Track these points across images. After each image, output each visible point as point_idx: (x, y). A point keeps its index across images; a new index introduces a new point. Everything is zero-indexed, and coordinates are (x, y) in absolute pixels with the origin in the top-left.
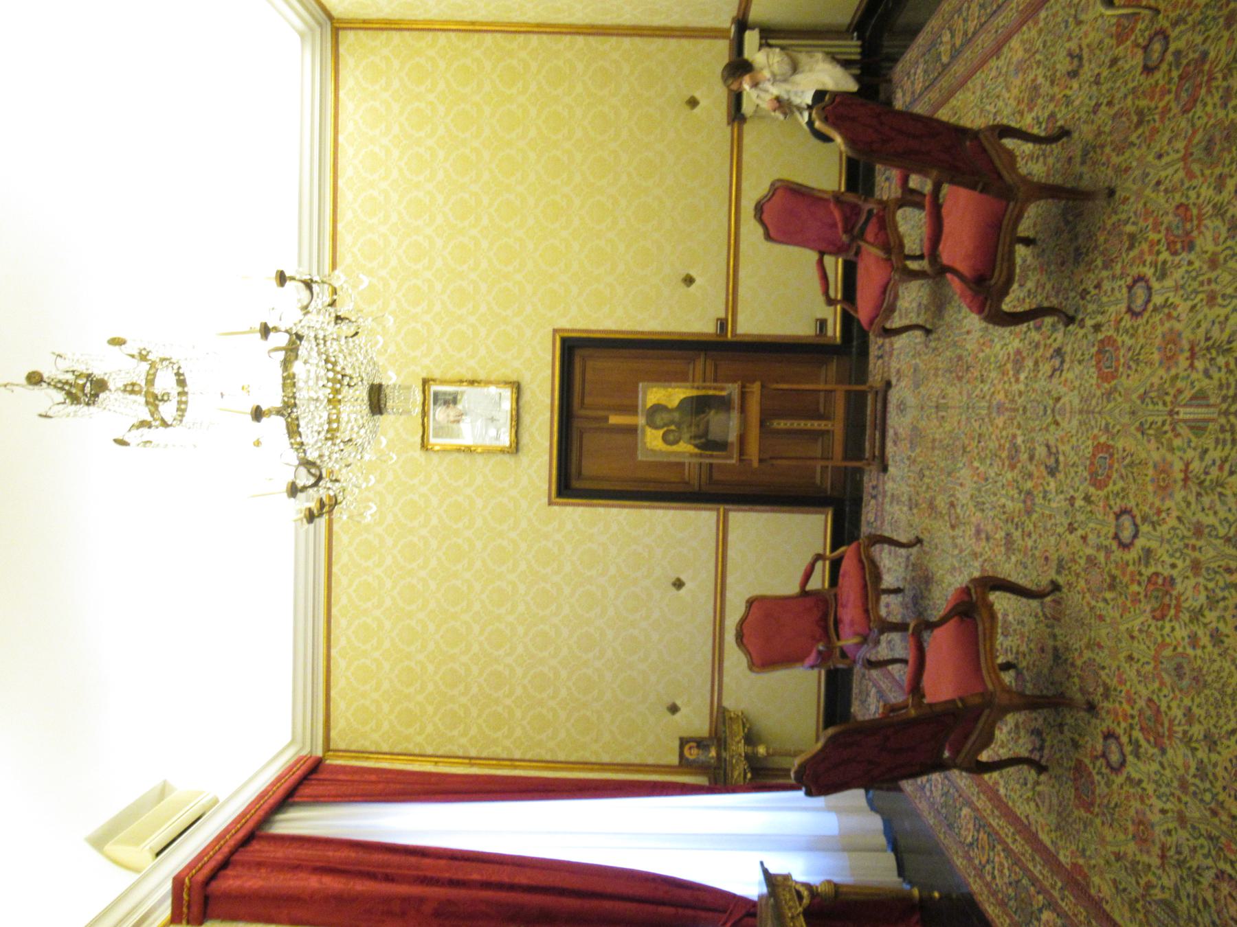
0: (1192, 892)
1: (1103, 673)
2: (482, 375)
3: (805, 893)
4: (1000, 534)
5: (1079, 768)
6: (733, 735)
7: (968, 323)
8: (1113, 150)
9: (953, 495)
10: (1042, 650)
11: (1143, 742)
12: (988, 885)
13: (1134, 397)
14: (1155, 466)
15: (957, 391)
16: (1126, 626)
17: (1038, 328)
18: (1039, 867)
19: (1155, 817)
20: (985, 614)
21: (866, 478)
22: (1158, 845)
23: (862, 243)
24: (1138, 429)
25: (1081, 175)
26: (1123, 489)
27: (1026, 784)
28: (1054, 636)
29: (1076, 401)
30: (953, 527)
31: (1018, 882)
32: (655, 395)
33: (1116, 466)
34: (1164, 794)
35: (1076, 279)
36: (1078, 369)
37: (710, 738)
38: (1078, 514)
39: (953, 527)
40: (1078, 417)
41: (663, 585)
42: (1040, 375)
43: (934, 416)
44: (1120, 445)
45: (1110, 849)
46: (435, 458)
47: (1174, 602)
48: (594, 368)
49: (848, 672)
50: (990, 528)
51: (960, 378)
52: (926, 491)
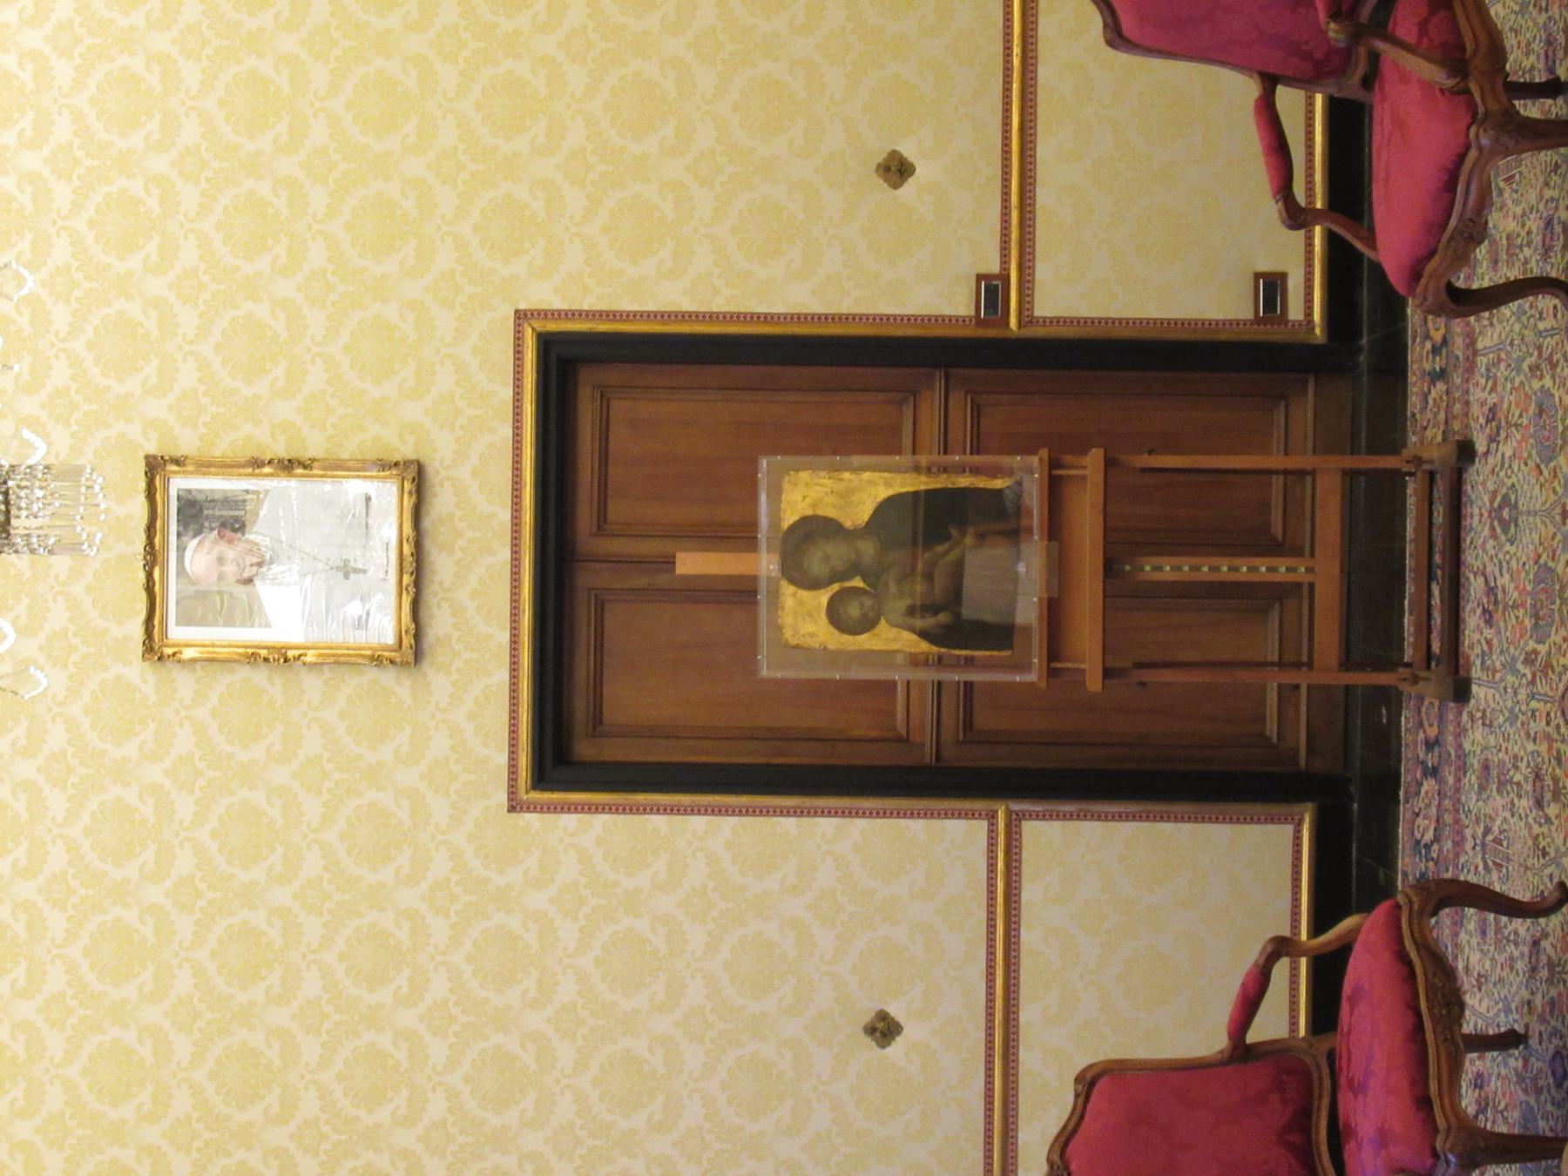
2: (314, 446)
21: (1406, 719)
23: (1380, 45)
32: (804, 492)
46: (184, 683)
48: (635, 424)
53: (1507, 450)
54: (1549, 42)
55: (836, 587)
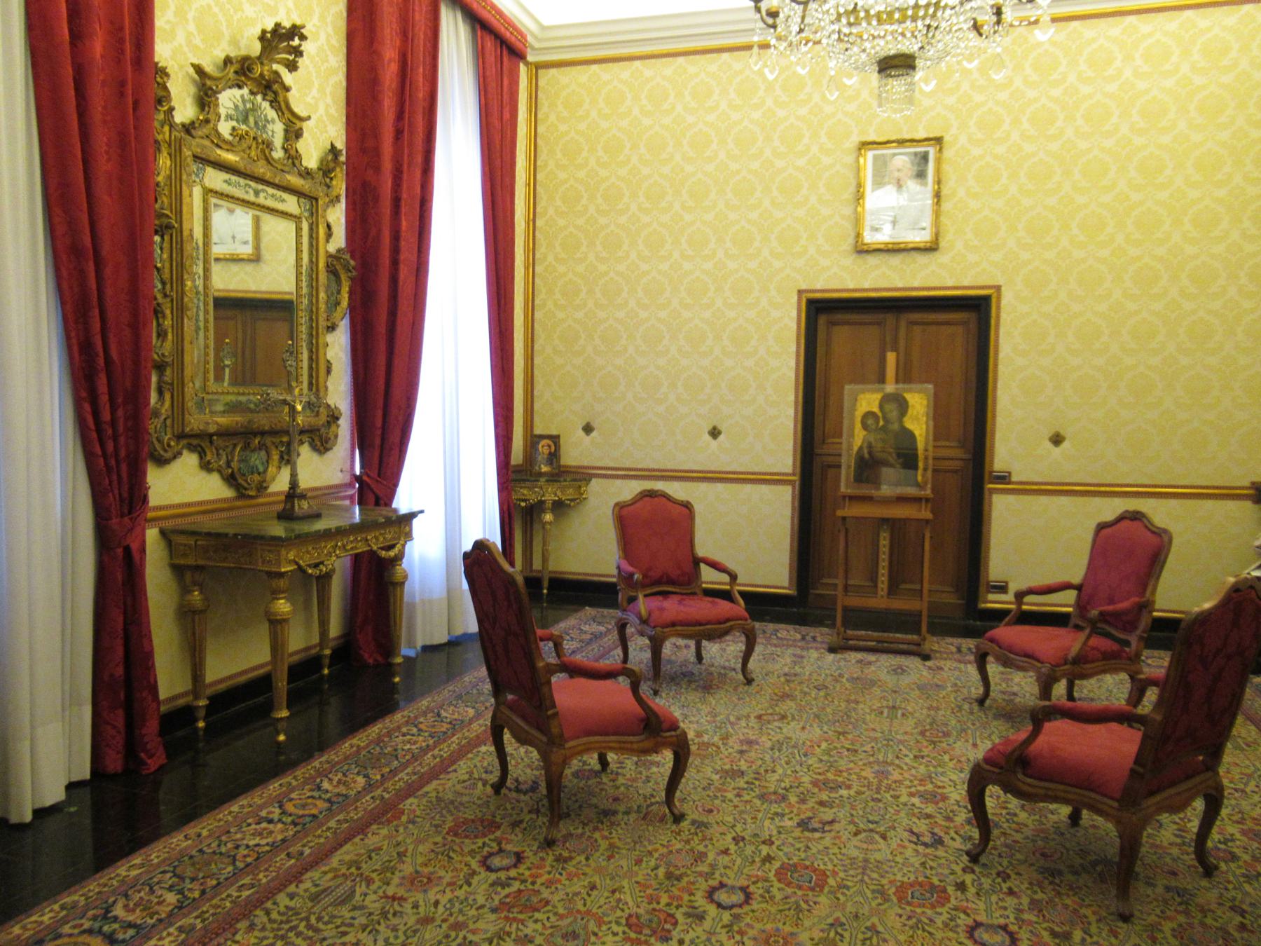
0: (356, 922)
1: (582, 858)
2: (946, 206)
3: (392, 553)
4: (743, 765)
5: (493, 825)
6: (563, 489)
7: (976, 745)
8: (1181, 925)
9: (793, 718)
10: (616, 799)
11: (507, 891)
12: (399, 728)
13: (875, 920)
14: (792, 934)
15: (909, 729)
16: (627, 886)
17: (969, 822)
18: (406, 778)
19: (432, 895)
20: (647, 744)
21: (825, 630)
22: (406, 895)
23: (1087, 631)
24: (837, 920)
25: (1154, 885)
26: (772, 898)
27: (486, 772)
28: (627, 813)
29: (878, 856)
30: (759, 717)
31: (396, 757)
32: (919, 403)
33: (800, 893)
34: (453, 906)
35: (1022, 869)
36: (916, 861)
37: (560, 466)
38: (753, 848)
39: (759, 717)
40: (861, 856)
41: (708, 411)
42: (915, 820)
43: (885, 703)
44: (823, 899)
45: (411, 848)
46: (850, 159)
47: (643, 939)
48: (952, 336)
49: (613, 604)
50: (753, 754)
51: (923, 733)
52: (802, 691)
53: (924, 673)
54: (1092, 700)
55: (880, 414)
